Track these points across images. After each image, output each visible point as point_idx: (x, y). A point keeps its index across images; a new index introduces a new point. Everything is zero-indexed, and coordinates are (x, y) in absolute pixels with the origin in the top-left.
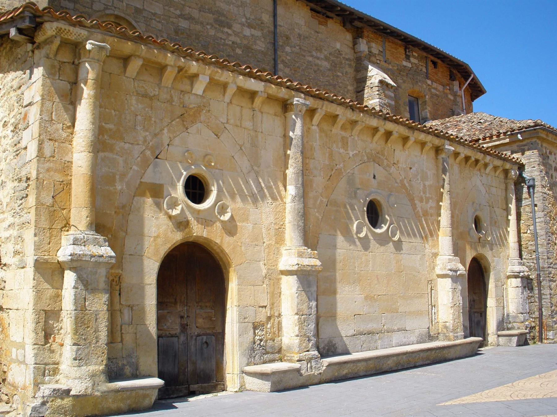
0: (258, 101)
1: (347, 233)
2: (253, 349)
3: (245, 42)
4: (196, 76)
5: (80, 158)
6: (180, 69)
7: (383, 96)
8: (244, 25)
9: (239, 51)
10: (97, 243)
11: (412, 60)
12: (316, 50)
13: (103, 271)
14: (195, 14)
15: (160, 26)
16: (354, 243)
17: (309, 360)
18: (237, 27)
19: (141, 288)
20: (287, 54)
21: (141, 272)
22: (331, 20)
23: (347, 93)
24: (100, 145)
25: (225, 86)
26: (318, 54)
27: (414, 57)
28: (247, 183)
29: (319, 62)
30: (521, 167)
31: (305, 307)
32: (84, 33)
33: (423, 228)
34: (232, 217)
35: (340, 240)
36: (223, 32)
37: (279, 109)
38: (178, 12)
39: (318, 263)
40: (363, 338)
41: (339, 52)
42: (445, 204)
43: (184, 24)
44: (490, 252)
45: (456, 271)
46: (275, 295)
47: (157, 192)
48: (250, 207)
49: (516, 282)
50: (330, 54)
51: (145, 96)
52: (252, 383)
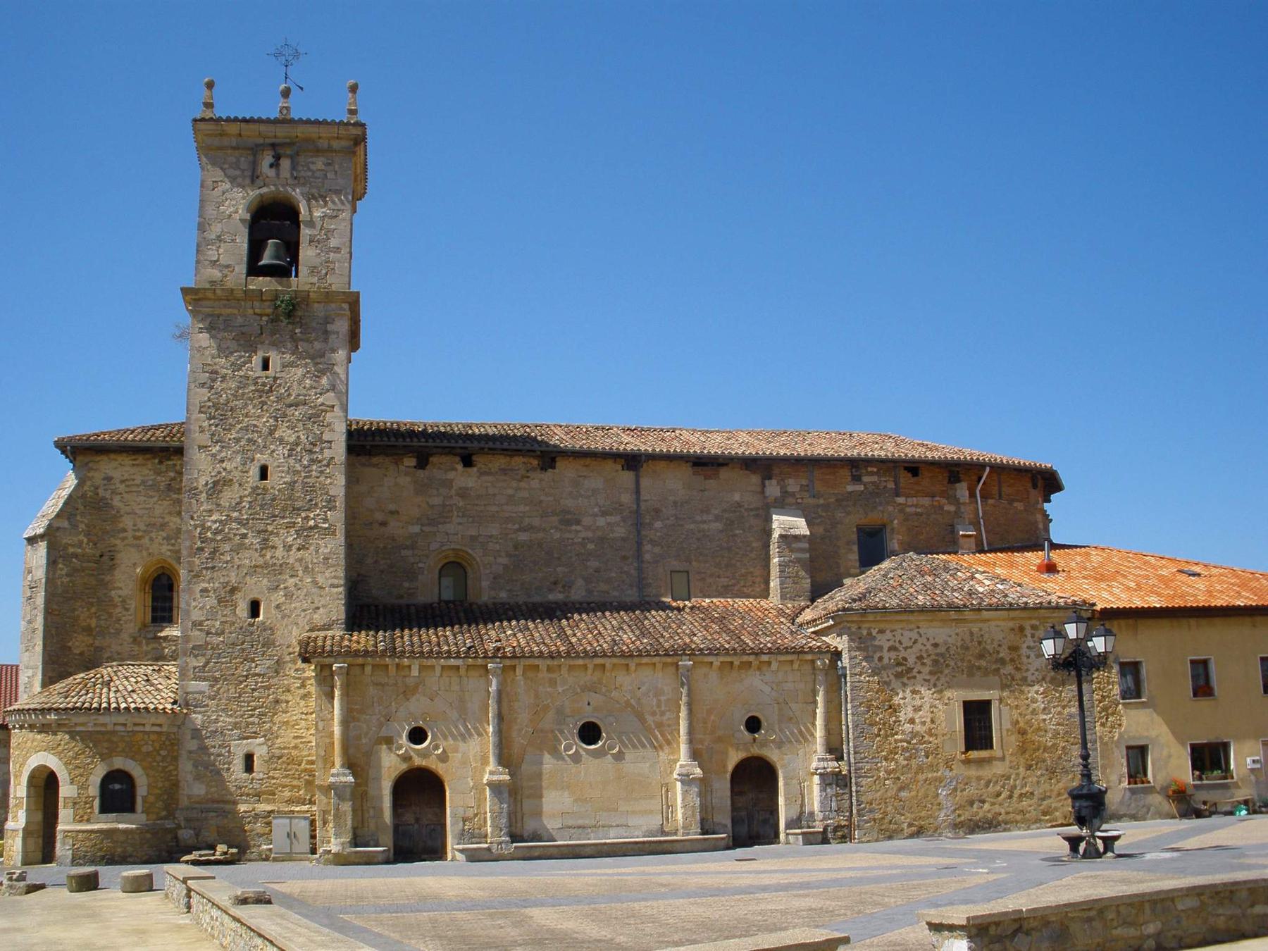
0: (462, 671)
1: (555, 752)
2: (462, 835)
3: (599, 533)
4: (409, 667)
5: (337, 730)
6: (398, 665)
7: (787, 552)
8: (596, 515)
9: (591, 546)
10: (344, 775)
11: (865, 479)
12: (702, 511)
13: (348, 791)
14: (536, 522)
15: (498, 547)
16: (563, 759)
17: (501, 843)
18: (587, 521)
19: (380, 798)
20: (656, 530)
21: (380, 789)
22: (725, 468)
23: (751, 551)
24: (345, 723)
25: (433, 667)
26: (705, 517)
27: (872, 474)
28: (456, 727)
29: (705, 526)
30: (837, 655)
31: (497, 807)
32: (332, 660)
33: (656, 739)
34: (444, 751)
35: (547, 758)
36: (570, 532)
37: (482, 671)
38: (517, 526)
39: (508, 777)
40: (572, 831)
41: (739, 505)
42: (683, 714)
43: (523, 537)
44: (777, 751)
45: (688, 775)
46: (481, 800)
47: (389, 741)
48: (461, 744)
49: (816, 779)
50: (724, 511)
51: (380, 684)
52: (459, 856)
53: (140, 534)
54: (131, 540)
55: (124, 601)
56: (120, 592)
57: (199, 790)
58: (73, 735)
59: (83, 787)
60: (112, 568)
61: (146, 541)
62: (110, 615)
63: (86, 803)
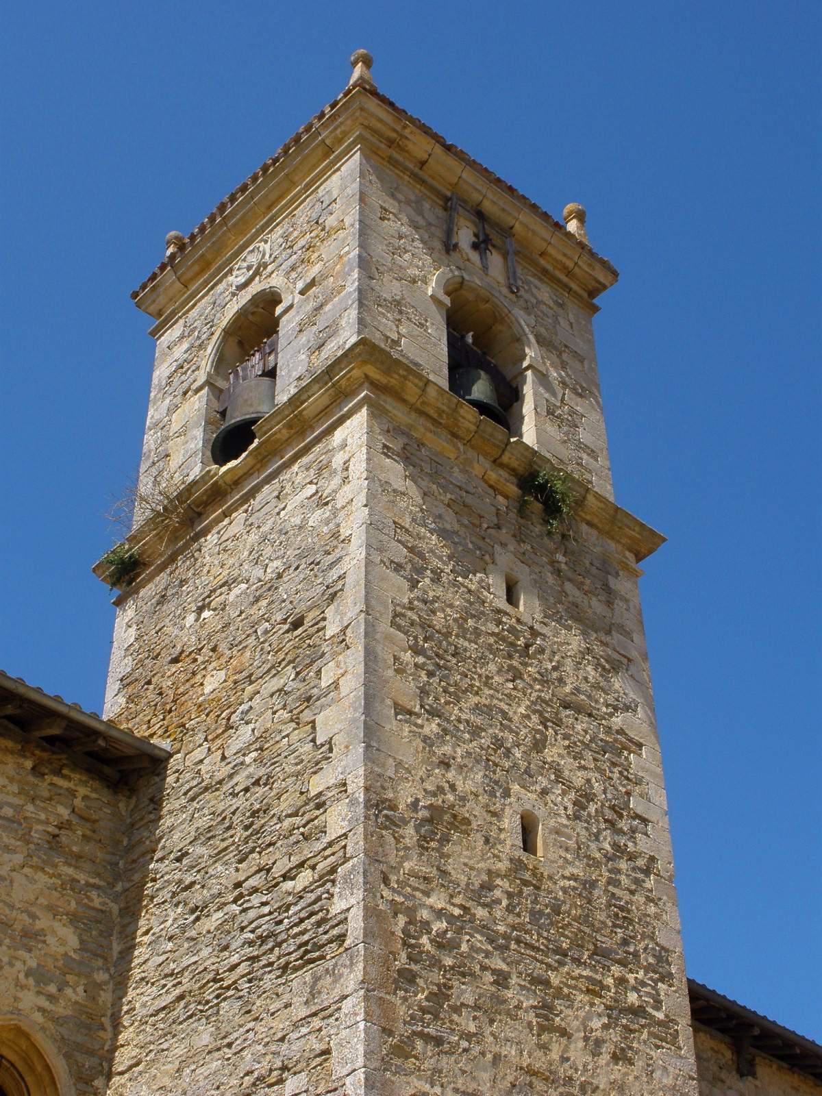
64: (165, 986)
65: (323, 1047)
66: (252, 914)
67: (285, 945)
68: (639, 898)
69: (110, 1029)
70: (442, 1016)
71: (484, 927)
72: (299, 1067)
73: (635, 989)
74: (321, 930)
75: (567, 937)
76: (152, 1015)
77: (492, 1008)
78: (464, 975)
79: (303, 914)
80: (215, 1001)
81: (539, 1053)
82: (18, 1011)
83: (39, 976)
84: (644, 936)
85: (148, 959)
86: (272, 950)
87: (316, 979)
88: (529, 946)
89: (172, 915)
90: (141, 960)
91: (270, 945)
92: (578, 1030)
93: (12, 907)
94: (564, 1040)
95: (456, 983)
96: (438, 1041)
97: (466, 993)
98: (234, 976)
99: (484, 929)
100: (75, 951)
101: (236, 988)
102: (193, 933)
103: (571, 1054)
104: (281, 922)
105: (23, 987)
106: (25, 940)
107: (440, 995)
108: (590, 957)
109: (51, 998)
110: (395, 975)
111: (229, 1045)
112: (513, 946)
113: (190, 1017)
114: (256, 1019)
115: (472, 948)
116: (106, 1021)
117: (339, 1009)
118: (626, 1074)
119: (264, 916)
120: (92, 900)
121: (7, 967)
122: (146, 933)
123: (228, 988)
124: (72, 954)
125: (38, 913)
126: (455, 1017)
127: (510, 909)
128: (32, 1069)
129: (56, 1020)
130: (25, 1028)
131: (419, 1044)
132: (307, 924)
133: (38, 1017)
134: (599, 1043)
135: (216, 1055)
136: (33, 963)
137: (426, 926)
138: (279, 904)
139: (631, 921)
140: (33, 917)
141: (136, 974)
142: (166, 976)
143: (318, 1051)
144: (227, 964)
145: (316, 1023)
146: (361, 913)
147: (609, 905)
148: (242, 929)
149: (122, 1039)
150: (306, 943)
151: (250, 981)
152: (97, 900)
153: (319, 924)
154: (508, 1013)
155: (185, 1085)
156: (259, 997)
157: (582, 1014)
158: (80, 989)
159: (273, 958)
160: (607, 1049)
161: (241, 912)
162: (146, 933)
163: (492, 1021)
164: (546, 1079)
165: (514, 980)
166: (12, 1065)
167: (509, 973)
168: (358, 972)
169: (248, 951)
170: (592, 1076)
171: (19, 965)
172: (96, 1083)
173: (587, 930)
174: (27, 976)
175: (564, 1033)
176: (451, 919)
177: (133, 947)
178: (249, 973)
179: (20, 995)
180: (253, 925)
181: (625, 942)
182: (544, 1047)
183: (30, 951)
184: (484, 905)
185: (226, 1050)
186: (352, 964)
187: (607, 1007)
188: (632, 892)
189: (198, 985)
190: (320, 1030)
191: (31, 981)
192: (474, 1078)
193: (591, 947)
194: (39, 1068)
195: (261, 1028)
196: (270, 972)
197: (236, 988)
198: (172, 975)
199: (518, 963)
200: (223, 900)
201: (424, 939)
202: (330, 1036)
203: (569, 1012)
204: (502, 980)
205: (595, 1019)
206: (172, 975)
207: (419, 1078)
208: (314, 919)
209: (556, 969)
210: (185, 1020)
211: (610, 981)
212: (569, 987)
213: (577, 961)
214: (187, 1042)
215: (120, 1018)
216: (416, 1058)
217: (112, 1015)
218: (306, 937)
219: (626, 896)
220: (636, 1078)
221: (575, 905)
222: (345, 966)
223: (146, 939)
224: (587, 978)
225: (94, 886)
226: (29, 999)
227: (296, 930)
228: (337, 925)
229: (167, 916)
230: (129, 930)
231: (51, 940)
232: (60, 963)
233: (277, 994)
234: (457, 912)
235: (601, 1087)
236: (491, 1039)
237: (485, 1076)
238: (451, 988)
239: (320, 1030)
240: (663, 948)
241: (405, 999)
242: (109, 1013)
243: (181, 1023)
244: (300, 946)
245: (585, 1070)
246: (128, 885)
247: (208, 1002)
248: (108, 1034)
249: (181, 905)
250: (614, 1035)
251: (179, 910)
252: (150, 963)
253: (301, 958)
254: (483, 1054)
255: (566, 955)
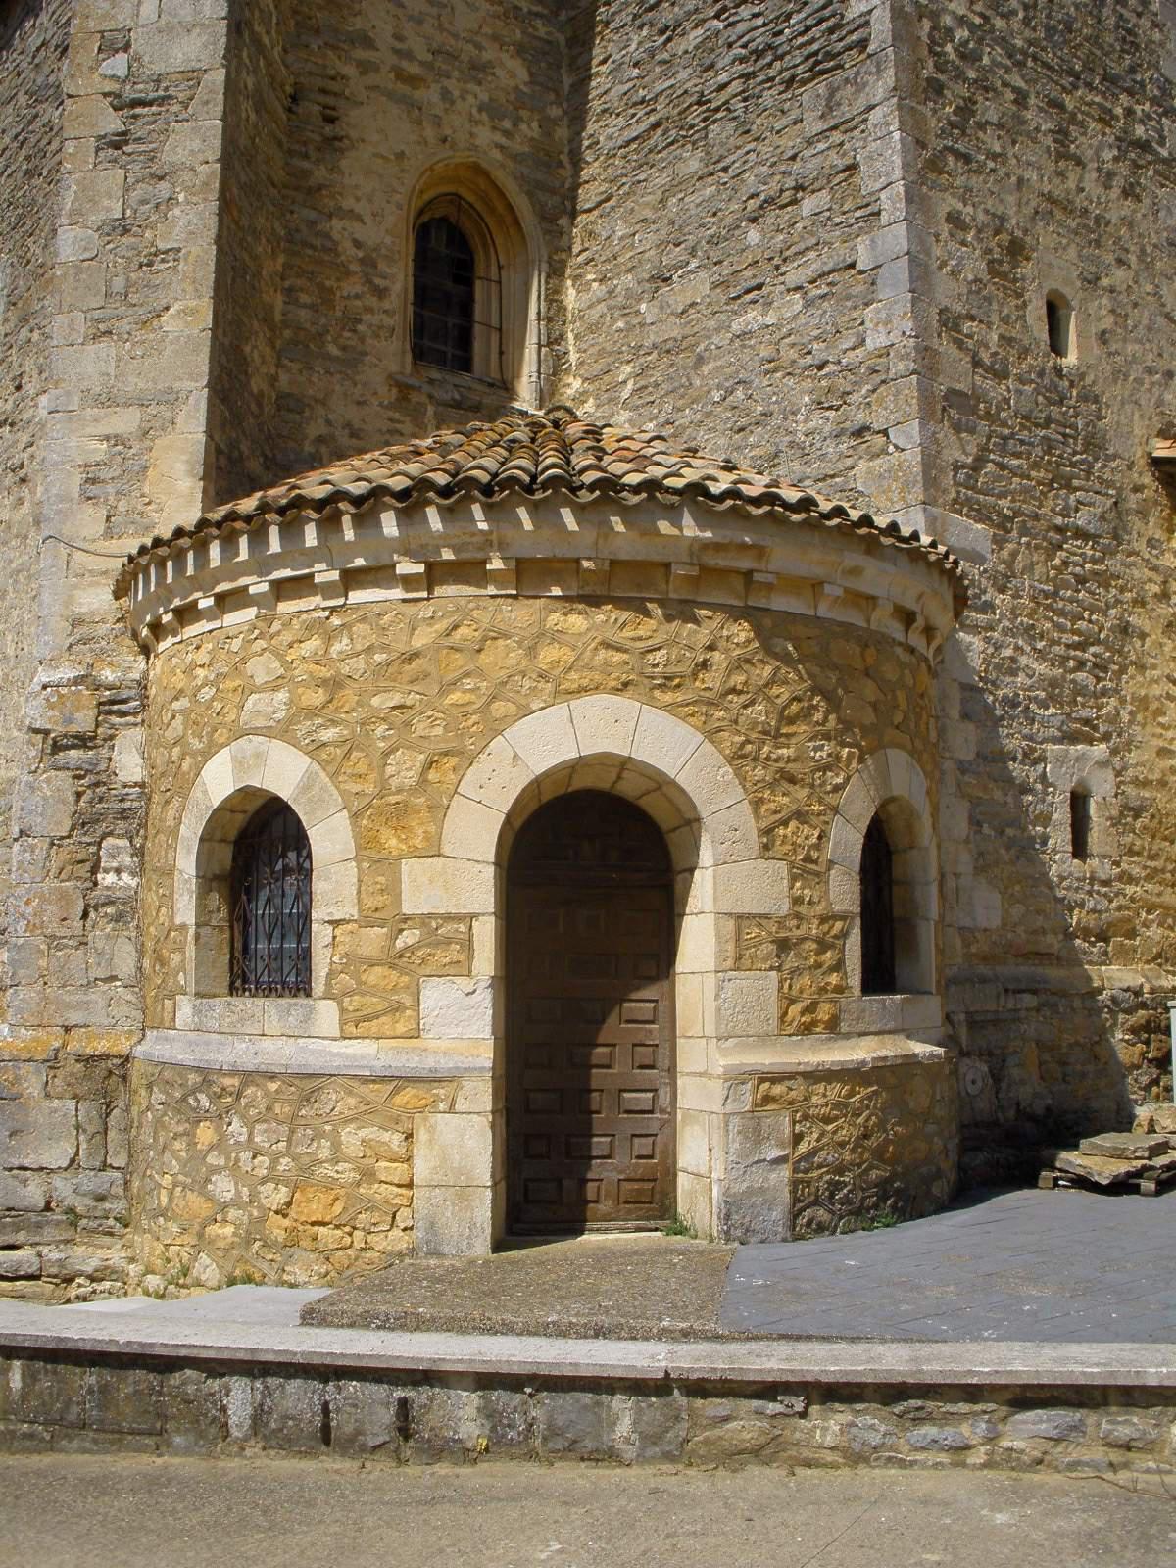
53: (414, 69)
54: (385, 79)
55: (369, 262)
56: (360, 232)
57: (987, 908)
58: (770, 629)
59: (808, 869)
60: (333, 145)
61: (430, 95)
62: (327, 296)
63: (823, 945)
64: (634, 115)
65: (848, 161)
66: (741, 28)
67: (788, 57)
68: (1145, 22)
69: (568, 166)
70: (968, 132)
71: (1003, 39)
72: (817, 186)
73: (1142, 122)
74: (834, 37)
75: (1078, 58)
76: (621, 148)
77: (1013, 128)
78: (986, 89)
79: (809, 22)
80: (702, 125)
81: (1057, 181)
82: (476, 148)
83: (492, 110)
84: (1150, 65)
85: (610, 89)
86: (770, 65)
87: (832, 91)
88: (1045, 65)
89: (636, 39)
90: (600, 91)
91: (769, 59)
92: (1092, 160)
93: (456, 36)
94: (1078, 169)
95: (980, 99)
96: (967, 158)
97: (989, 110)
98: (724, 96)
99: (1003, 41)
100: (526, 84)
101: (728, 109)
102: (666, 56)
103: (1087, 185)
104: (781, 33)
105: (477, 123)
106: (474, 73)
107: (966, 110)
108: (1101, 83)
109: (507, 134)
110: (924, 84)
111: (725, 170)
112: (1030, 63)
113: (672, 144)
114: (757, 139)
115: (993, 61)
116: (564, 158)
117: (866, 120)
118: (1134, 211)
119: (757, 28)
120: (537, 30)
121: (459, 101)
122: (604, 61)
123: (717, 110)
124: (522, 87)
125: (484, 44)
126: (981, 134)
127: (1026, 22)
128: (492, 210)
129: (516, 157)
130: (484, 164)
131: (951, 159)
132: (815, 32)
133: (496, 155)
134: (1110, 175)
135: (710, 180)
136: (484, 97)
137: (949, 31)
138: (777, 13)
139: (1137, 47)
140: (479, 47)
141: (596, 106)
142: (635, 104)
143: (841, 167)
144: (713, 84)
145: (836, 137)
146: (888, 14)
147: (1118, 27)
148: (730, 46)
149: (585, 174)
150: (816, 53)
151: (745, 100)
152: (542, 30)
153: (831, 31)
154: (1028, 135)
155: (671, 215)
156: (759, 115)
157: (1094, 142)
158: (535, 125)
159: (773, 72)
160: (1118, 183)
161: (726, 27)
162: (604, 61)
163: (1014, 143)
164: (1065, 208)
165: (1032, 101)
166: (471, 206)
167: (1028, 92)
168: (889, 76)
169: (739, 68)
170: (1105, 209)
171: (471, 99)
172: (560, 222)
173: (1098, 53)
174: (480, 110)
175: (1079, 162)
176: (972, 27)
177: (589, 78)
178: (743, 92)
179: (475, 130)
180: (745, 39)
181: (1132, 70)
182: (1061, 174)
183: (480, 84)
184: (1003, 16)
185: (721, 174)
186: (879, 71)
187: (1118, 139)
188: (1139, 15)
189: (676, 111)
190: (841, 144)
191: (485, 116)
192: (1001, 201)
193: (1101, 72)
194: (500, 208)
195: (765, 149)
196: (770, 88)
197: (728, 109)
198: (642, 102)
199: (1035, 82)
200: (701, 16)
201: (949, 48)
202: (855, 150)
203: (1082, 139)
204: (1021, 100)
205: (1107, 150)
206: (642, 102)
207: (953, 195)
208: (824, 26)
209: (1069, 93)
210: (664, 148)
211: (1119, 111)
212: (1083, 112)
213: (1089, 86)
214: (670, 170)
215: (581, 153)
216: (949, 175)
217: (571, 151)
218: (815, 47)
219: (1134, 19)
220: (1144, 215)
221: (1084, 23)
222: (870, 74)
223: (603, 68)
224: (1098, 104)
225: (537, 14)
226: (485, 136)
227: (800, 40)
228: (856, 30)
229: (629, 40)
230: (580, 61)
231: (499, 72)
232: (512, 97)
233: (783, 111)
234: (978, 20)
235: (1114, 221)
236: (1015, 161)
237: (1011, 199)
238: (975, 103)
239: (841, 144)
240: (1167, 80)
241: (935, 111)
242: (567, 150)
243: (660, 152)
244: (807, 58)
245: (1099, 203)
246: (573, 13)
247: (692, 127)
248: (567, 172)
249: (646, 28)
250: (1123, 169)
251: (644, 33)
252: (613, 92)
253: (811, 70)
254: (1008, 175)
255: (1078, 79)
